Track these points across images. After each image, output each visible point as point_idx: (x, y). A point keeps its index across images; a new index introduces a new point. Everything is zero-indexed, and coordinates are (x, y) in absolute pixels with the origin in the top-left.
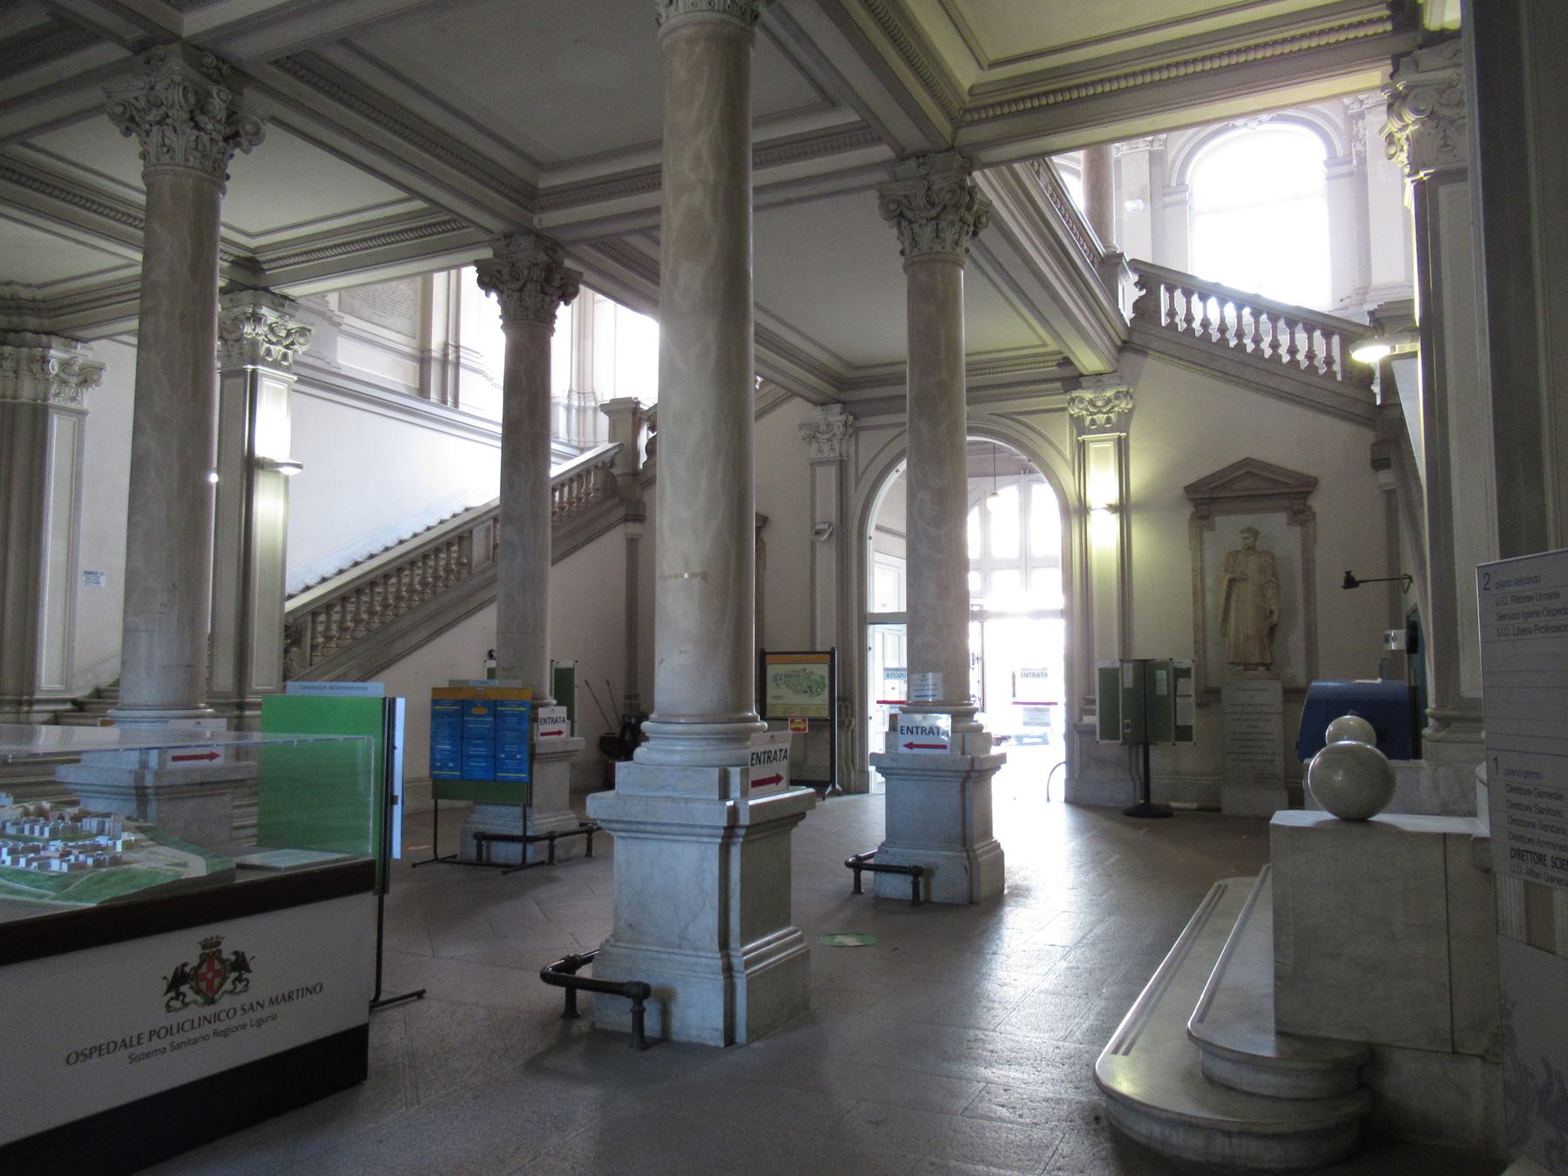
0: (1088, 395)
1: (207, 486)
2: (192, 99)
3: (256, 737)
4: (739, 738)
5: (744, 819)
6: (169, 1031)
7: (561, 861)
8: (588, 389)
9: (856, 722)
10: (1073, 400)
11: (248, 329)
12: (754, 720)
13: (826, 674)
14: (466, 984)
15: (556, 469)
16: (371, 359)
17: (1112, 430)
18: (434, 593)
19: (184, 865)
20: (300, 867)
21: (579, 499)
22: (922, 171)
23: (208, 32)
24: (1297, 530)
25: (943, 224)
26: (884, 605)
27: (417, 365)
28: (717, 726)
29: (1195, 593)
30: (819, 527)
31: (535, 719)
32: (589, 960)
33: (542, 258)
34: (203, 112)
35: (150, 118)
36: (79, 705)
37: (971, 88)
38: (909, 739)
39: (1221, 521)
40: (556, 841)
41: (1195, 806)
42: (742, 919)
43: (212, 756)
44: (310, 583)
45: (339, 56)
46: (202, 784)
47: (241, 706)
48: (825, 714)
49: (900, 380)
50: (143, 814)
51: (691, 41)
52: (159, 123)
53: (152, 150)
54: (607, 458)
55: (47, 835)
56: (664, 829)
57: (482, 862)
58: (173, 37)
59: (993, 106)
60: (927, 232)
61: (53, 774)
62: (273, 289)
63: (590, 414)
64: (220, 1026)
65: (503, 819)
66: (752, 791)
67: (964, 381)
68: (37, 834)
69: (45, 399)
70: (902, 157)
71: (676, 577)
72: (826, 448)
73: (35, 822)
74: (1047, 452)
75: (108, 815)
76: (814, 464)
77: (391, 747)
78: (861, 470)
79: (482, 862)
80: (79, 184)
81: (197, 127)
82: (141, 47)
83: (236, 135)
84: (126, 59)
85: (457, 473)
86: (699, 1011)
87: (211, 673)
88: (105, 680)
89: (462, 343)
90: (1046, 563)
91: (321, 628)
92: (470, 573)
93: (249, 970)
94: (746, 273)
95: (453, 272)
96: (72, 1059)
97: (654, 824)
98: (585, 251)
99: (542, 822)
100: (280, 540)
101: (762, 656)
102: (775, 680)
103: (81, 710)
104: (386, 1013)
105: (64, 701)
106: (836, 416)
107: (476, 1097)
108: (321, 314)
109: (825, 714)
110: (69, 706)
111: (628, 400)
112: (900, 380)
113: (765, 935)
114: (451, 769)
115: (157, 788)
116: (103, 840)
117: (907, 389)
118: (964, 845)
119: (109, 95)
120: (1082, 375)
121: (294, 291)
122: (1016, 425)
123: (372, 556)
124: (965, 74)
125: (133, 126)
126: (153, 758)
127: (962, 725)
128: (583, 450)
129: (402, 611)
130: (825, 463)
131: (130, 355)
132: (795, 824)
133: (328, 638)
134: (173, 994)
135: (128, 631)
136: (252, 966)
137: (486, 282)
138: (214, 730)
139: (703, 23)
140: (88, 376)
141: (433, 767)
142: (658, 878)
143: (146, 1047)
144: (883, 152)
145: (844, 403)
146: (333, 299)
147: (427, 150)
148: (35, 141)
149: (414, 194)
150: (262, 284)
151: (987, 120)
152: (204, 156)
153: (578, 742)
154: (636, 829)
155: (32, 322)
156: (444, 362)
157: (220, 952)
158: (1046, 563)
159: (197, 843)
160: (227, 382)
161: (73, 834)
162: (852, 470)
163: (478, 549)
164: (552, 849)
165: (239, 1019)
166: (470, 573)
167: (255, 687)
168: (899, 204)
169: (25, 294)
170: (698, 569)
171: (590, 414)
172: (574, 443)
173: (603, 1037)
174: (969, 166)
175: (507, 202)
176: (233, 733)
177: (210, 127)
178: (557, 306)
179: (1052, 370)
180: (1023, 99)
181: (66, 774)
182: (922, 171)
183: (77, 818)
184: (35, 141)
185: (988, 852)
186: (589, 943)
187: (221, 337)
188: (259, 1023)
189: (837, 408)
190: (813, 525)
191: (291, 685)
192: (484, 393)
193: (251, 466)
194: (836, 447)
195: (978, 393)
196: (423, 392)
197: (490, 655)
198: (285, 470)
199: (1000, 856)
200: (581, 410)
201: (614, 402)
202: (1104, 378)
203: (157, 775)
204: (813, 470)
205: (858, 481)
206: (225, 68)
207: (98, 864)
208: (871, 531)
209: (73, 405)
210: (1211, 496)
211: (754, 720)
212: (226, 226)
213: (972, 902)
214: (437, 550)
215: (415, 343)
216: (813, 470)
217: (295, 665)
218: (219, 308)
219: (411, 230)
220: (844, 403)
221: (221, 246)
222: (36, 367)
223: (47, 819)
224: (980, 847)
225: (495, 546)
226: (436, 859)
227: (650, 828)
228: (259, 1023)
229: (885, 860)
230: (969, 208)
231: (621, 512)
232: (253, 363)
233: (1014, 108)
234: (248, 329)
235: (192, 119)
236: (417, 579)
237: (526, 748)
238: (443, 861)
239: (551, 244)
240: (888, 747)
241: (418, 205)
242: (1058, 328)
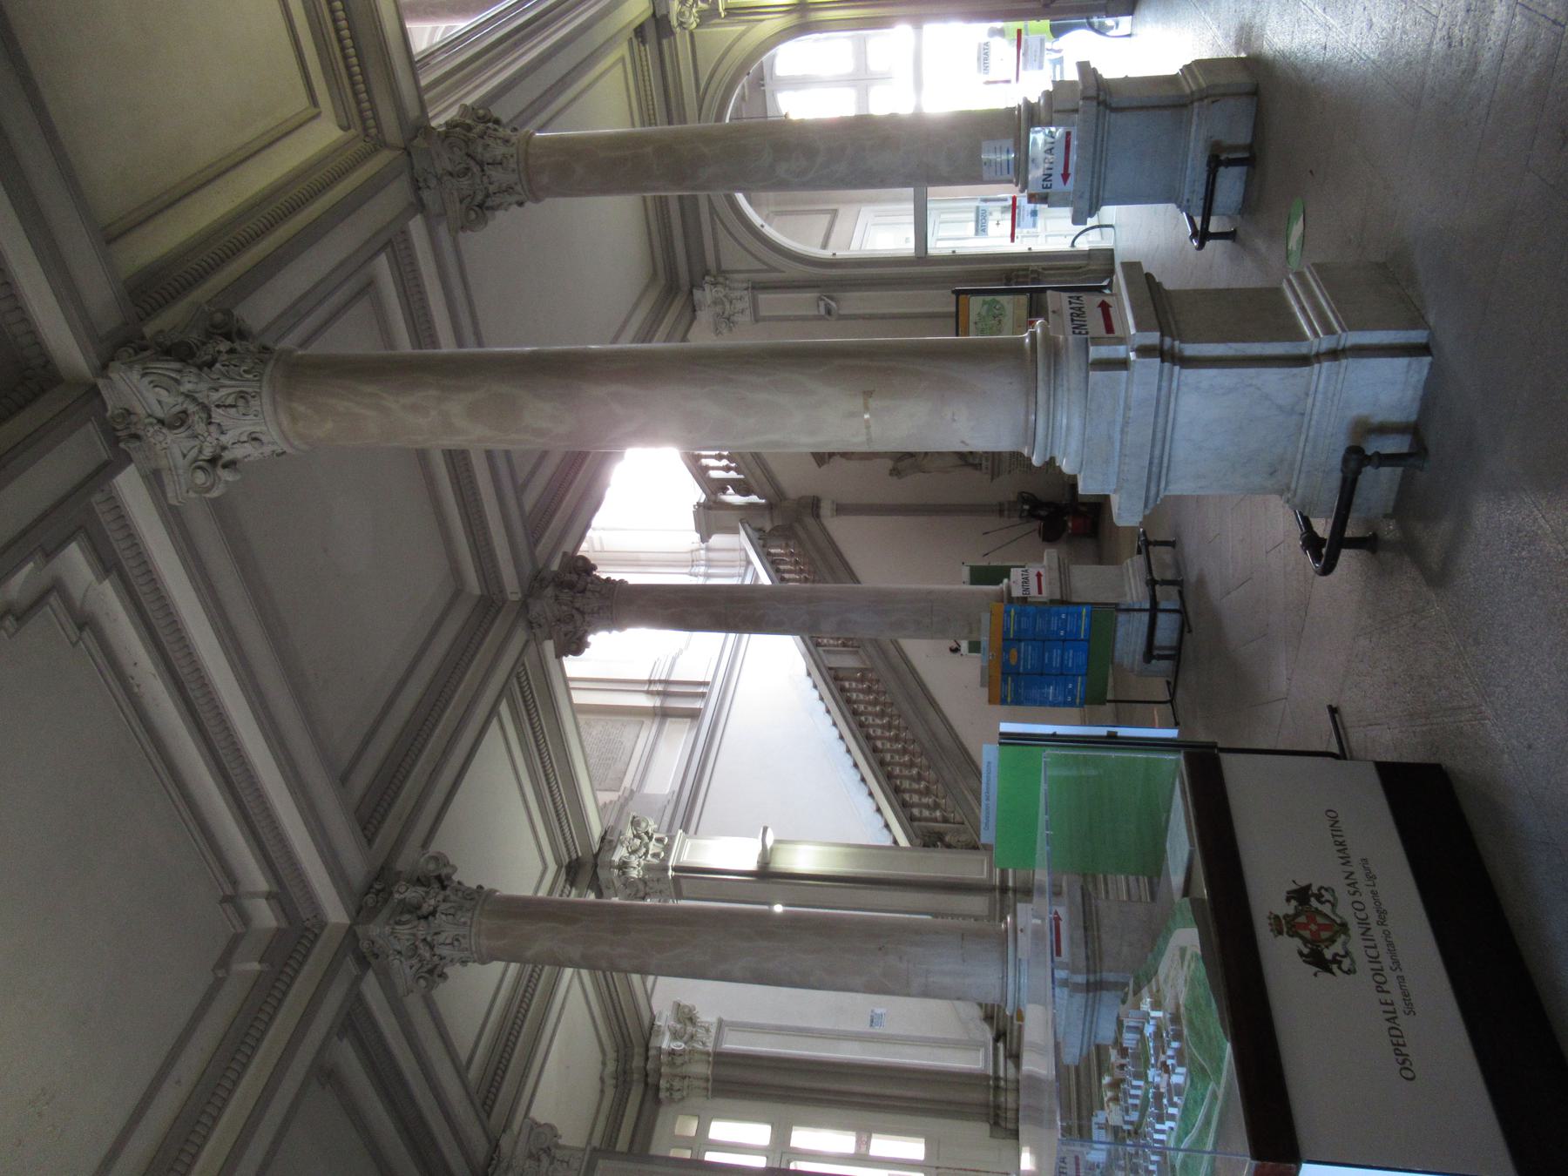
1: (785, 912)
2: (406, 917)
3: (1042, 876)
4: (1054, 352)
5: (1153, 338)
6: (1378, 972)
7: (1179, 571)
8: (688, 556)
9: (1033, 265)
10: (681, 24)
11: (634, 874)
12: (1033, 336)
13: (980, 299)
14: (1329, 660)
15: (765, 580)
16: (664, 763)
18: (892, 704)
19: (1183, 951)
20: (1189, 830)
21: (797, 563)
22: (433, 183)
23: (344, 903)
25: (488, 157)
26: (907, 240)
27: (669, 720)
28: (1040, 376)
30: (822, 311)
31: (1024, 600)
32: (1306, 521)
33: (550, 591)
34: (419, 907)
35: (427, 955)
36: (1000, 1036)
37: (342, 128)
38: (1057, 180)
40: (1157, 577)
42: (1272, 340)
43: (1057, 919)
44: (882, 824)
45: (361, 779)
46: (1086, 929)
47: (1004, 889)
48: (1024, 299)
49: (662, 203)
50: (1120, 986)
51: (294, 418)
52: (432, 947)
53: (457, 955)
54: (755, 536)
55: (1141, 1083)
56: (1159, 435)
57: (1176, 655)
58: (351, 932)
59: (358, 102)
60: (496, 174)
61: (1068, 1067)
62: (596, 848)
63: (712, 555)
64: (1373, 918)
65: (1129, 636)
66: (1118, 332)
67: (661, 128)
68: (1139, 1092)
69: (708, 1054)
70: (420, 206)
71: (868, 427)
72: (739, 305)
73: (1126, 1093)
74: (738, 53)
75: (1120, 1023)
76: (757, 319)
77: (1054, 737)
78: (759, 266)
79: (1176, 655)
80: (504, 1017)
81: (433, 913)
82: (363, 962)
83: (439, 878)
84: (376, 974)
85: (772, 675)
86: (1384, 388)
87: (970, 916)
88: (977, 1013)
89: (646, 677)
90: (861, 54)
91: (926, 813)
92: (871, 670)
93: (1309, 887)
94: (533, 352)
95: (572, 685)
96: (1410, 1075)
97: (1153, 446)
98: (542, 549)
99: (1135, 592)
100: (826, 849)
103: (1005, 1034)
104: (1353, 744)
105: (996, 1049)
106: (705, 295)
107: (1477, 643)
108: (622, 807)
109: (1024, 299)
110: (1001, 1046)
111: (697, 514)
112: (662, 203)
113: (1293, 315)
114: (1075, 686)
115: (1088, 972)
116: (1149, 1030)
117: (673, 194)
118: (1184, 106)
119: (410, 991)
120: (654, 15)
121: (596, 831)
123: (856, 765)
124: (325, 134)
125: (437, 971)
126: (1061, 974)
127: (1043, 115)
128: (749, 562)
129: (910, 736)
130: (755, 305)
131: (663, 981)
132: (1159, 285)
133: (936, 806)
134: (1335, 967)
135: (926, 993)
136: (1303, 883)
137: (576, 645)
138: (1029, 917)
139: (274, 402)
140: (686, 1016)
141: (1072, 704)
142: (1212, 450)
143: (1396, 996)
144: (416, 226)
145: (692, 286)
146: (605, 797)
147: (448, 702)
148: (464, 1057)
149: (493, 711)
150: (591, 859)
151: (374, 109)
152: (460, 908)
153: (1051, 555)
154: (1157, 469)
155: (637, 1062)
156: (664, 694)
157: (1286, 916)
158: (861, 54)
159: (1154, 937)
160: (685, 893)
161: (1141, 1059)
163: (847, 661)
164: (1165, 582)
165: (1366, 898)
166: (871, 670)
167: (985, 876)
168: (469, 208)
169: (611, 1067)
170: (860, 402)
171: (712, 555)
172: (742, 570)
173: (1405, 505)
174: (422, 128)
175: (498, 622)
176: (1035, 899)
177: (432, 902)
178: (598, 578)
179: (649, 50)
180: (348, 67)
181: (1072, 1055)
182: (433, 183)
183: (1123, 1052)
184: (464, 1057)
185: (1194, 78)
186: (1281, 524)
187: (643, 898)
188: (1371, 877)
189: (697, 294)
190: (819, 318)
191: (986, 837)
192: (692, 653)
193: (765, 874)
194: (738, 294)
195: (672, 107)
196: (694, 715)
197: (955, 650)
198: (769, 843)
199: (1199, 63)
200: (709, 563)
201: (698, 529)
202: (608, 837)
203: (1074, 971)
204: (765, 319)
205: (774, 270)
206: (377, 886)
207: (1178, 1036)
208: (826, 254)
209: (713, 1031)
211: (1033, 336)
212: (537, 889)
213: (1255, 93)
214: (849, 701)
215: (647, 722)
216: (765, 319)
217: (963, 838)
218: (616, 900)
219: (530, 720)
220: (692, 286)
221: (556, 896)
222: (679, 1061)
223: (1123, 1081)
224: (1188, 87)
225: (844, 645)
226: (1171, 702)
227: (1157, 452)
228: (1371, 877)
229: (1198, 202)
230: (469, 128)
231: (809, 521)
232: (666, 869)
233: (356, 69)
234: (634, 874)
235: (426, 918)
236: (878, 721)
237: (1055, 609)
238: (1173, 694)
239: (537, 582)
240: (1065, 205)
241: (504, 709)
242: (600, 40)
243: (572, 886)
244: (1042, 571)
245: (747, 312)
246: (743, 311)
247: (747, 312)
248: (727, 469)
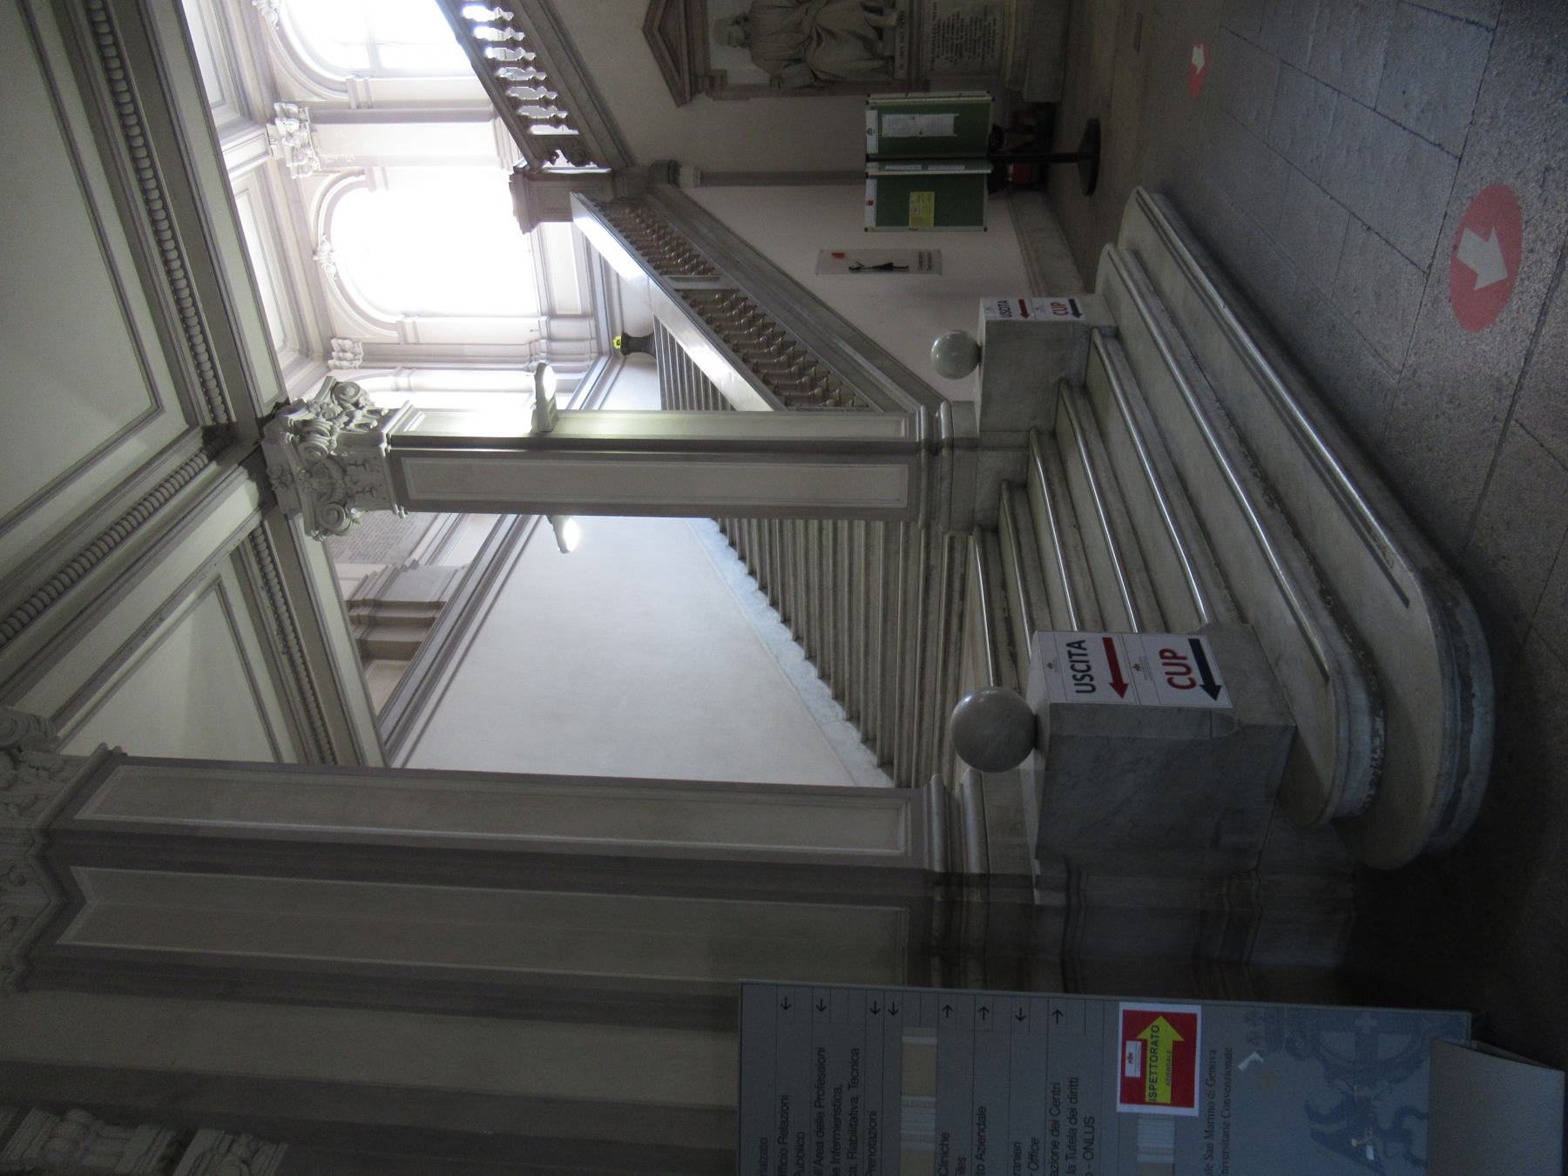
8: (525, 350)
63: (555, 345)
231: (667, 188)
243: (211, 458)
248: (556, 122)
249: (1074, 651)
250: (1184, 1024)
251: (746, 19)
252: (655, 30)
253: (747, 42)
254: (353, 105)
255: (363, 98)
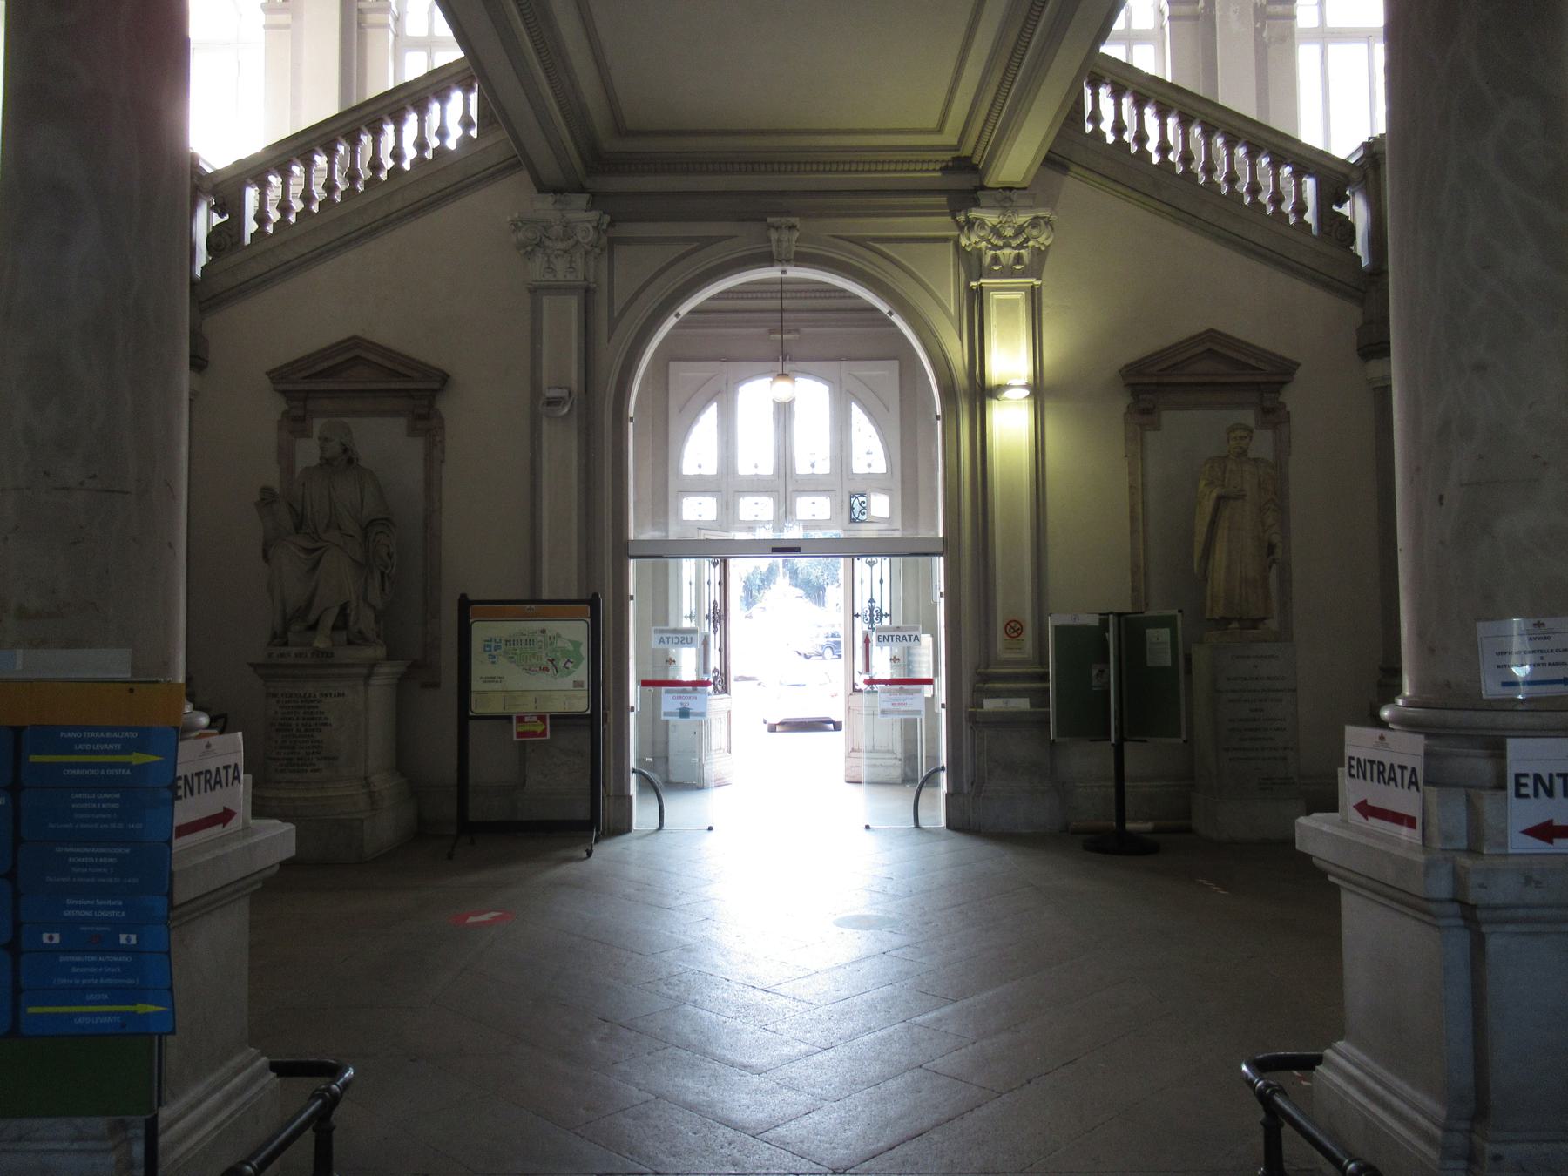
0: (992, 218)
17: (1023, 274)
24: (418, 444)
29: (1133, 519)
39: (1168, 417)
41: (1149, 826)
48: (581, 705)
72: (560, 265)
78: (619, 304)
101: (465, 604)
102: (487, 648)
106: (581, 216)
109: (581, 705)
122: (868, 254)
162: (603, 313)
189: (582, 200)
194: (579, 262)
202: (1015, 195)
205: (613, 324)
210: (1144, 384)
244: (235, 824)
245: (549, 277)
246: (550, 269)
247: (549, 277)
248: (261, 218)
249: (231, 771)
250: (543, 733)
251: (350, 461)
252: (357, 352)
253: (326, 462)
254: (362, 5)
255: (372, 18)
